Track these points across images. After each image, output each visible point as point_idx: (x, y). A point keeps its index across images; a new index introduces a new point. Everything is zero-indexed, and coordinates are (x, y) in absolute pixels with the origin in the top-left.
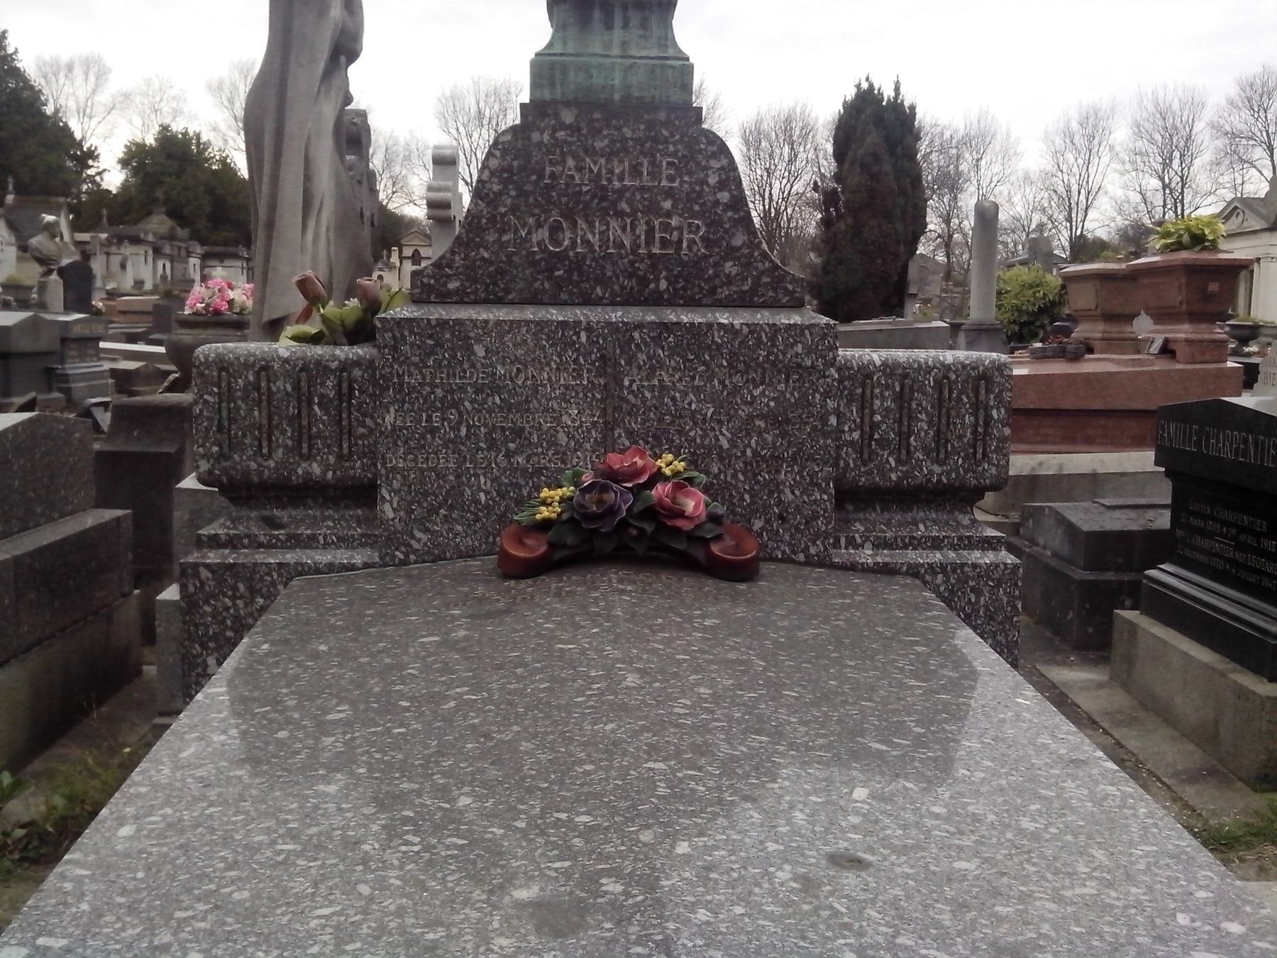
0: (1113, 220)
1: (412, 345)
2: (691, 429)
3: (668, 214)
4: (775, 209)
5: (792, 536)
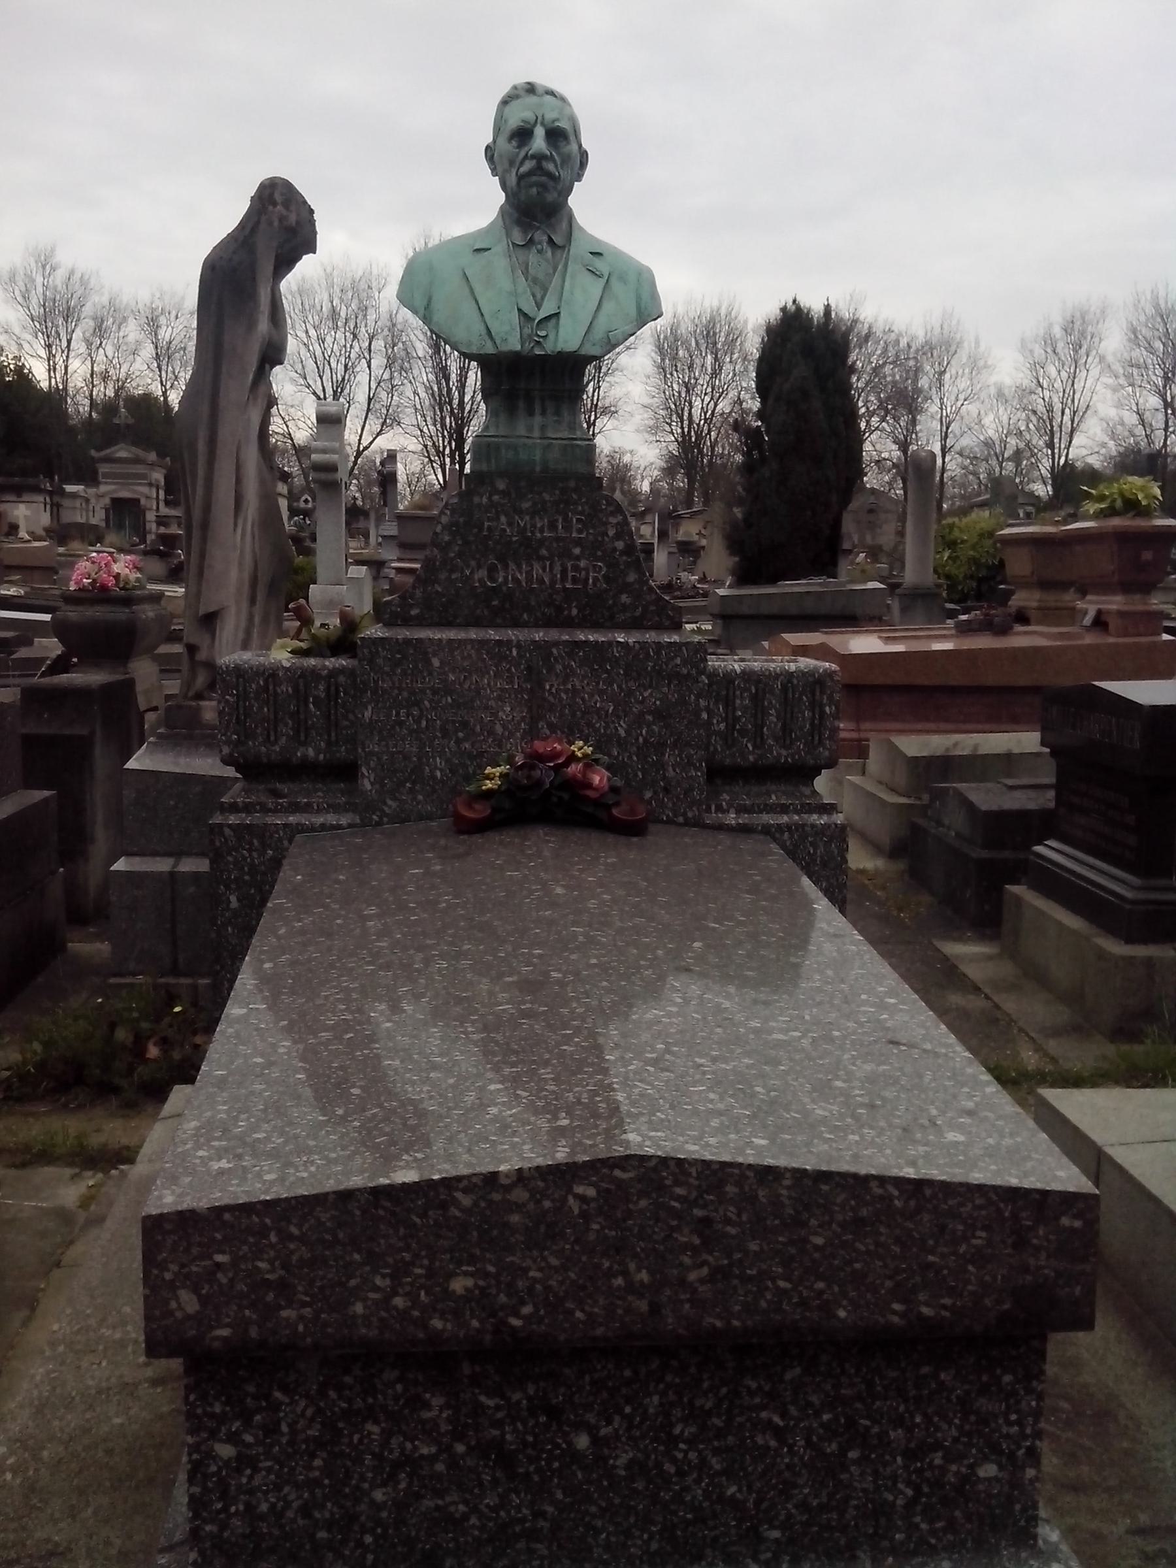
0: (1104, 445)
1: (385, 658)
2: (597, 722)
3: (578, 558)
4: (696, 433)
5: (674, 804)
